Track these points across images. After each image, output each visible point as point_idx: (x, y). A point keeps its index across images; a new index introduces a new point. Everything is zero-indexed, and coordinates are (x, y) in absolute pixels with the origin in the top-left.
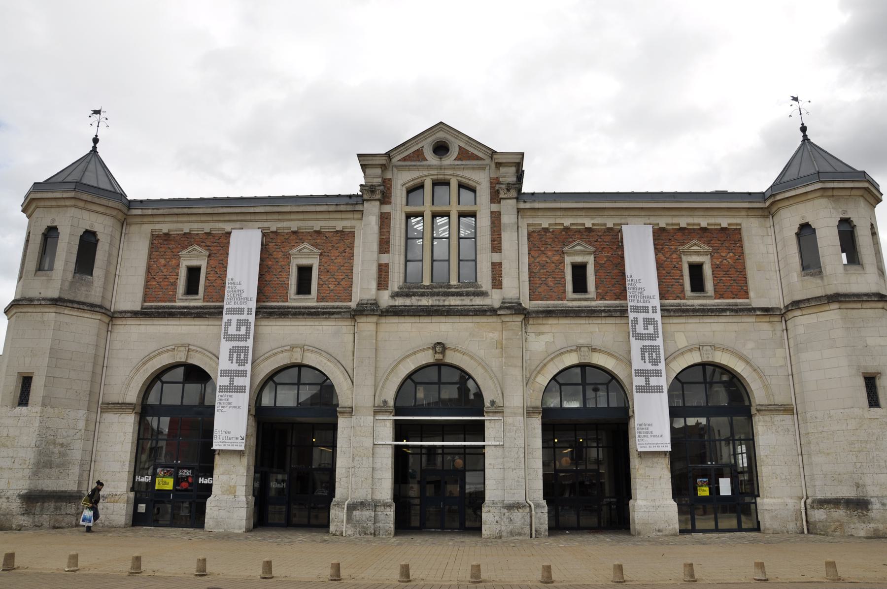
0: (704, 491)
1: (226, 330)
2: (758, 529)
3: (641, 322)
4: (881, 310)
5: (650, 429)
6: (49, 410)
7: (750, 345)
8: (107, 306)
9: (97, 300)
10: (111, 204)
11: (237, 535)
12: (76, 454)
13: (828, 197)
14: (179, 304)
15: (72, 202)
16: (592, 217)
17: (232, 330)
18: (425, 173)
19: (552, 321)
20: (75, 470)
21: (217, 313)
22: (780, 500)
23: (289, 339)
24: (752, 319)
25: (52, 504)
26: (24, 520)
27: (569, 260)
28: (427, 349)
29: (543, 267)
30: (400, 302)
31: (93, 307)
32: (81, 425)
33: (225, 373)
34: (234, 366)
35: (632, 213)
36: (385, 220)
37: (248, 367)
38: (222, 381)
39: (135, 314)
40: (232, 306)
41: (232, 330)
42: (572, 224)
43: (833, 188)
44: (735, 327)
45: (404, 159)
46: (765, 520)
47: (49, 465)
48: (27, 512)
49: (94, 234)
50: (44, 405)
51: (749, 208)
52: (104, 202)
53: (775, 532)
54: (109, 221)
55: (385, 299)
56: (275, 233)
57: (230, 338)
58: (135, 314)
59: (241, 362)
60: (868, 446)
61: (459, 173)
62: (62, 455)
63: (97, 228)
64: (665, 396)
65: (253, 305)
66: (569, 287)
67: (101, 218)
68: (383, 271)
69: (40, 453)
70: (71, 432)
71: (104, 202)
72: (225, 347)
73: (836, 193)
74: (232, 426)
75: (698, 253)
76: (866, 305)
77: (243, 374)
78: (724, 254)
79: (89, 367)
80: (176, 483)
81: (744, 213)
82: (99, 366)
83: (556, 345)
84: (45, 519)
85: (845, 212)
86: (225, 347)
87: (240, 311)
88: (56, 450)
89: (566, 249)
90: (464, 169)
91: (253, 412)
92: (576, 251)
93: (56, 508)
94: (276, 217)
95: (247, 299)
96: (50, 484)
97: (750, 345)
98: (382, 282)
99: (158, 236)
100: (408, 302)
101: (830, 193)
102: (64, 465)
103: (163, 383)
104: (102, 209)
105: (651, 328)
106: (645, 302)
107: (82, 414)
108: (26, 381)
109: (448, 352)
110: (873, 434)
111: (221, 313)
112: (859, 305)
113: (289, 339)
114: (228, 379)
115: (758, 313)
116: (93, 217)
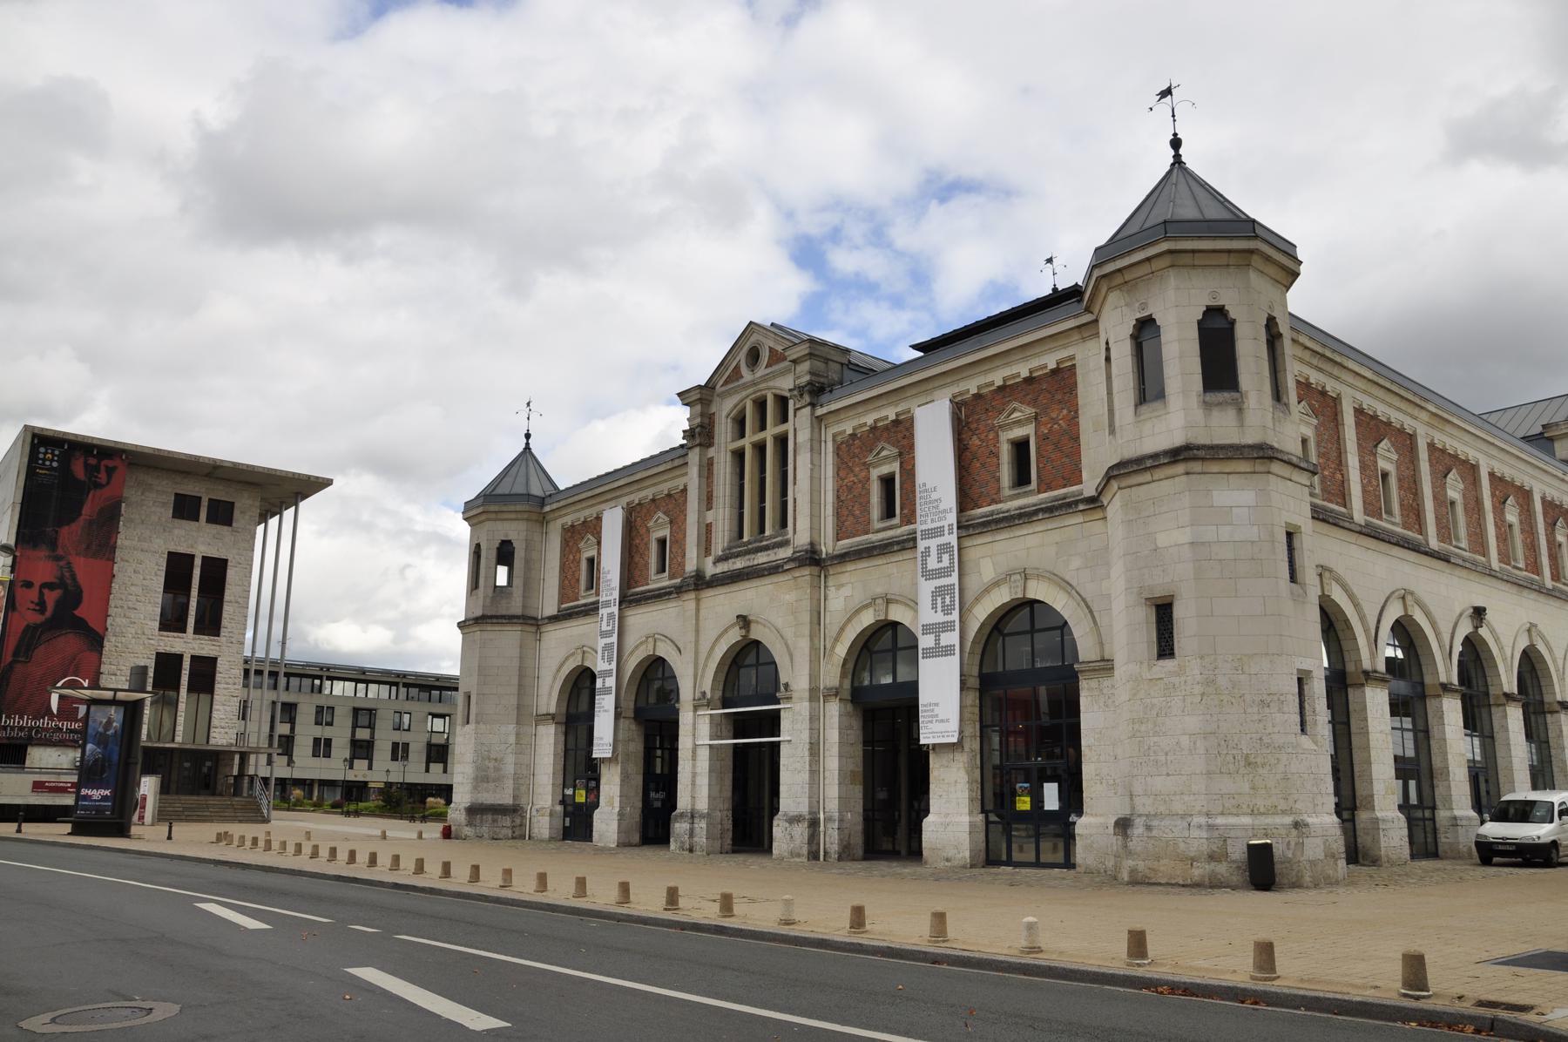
0: (1024, 804)
1: (924, 563)
2: (1069, 864)
3: (934, 552)
4: (1184, 478)
5: (937, 710)
6: (482, 726)
7: (1076, 563)
8: (532, 613)
9: (518, 612)
10: (519, 508)
11: (610, 849)
12: (509, 768)
13: (1119, 287)
14: (582, 602)
15: (483, 517)
16: (1026, 359)
17: (932, 563)
18: (744, 394)
19: (850, 567)
20: (509, 784)
21: (909, 543)
22: (1101, 820)
23: (1007, 565)
24: (1079, 519)
25: (490, 817)
26: (468, 831)
27: (875, 473)
28: (732, 626)
29: (850, 489)
30: (723, 567)
31: (510, 619)
32: (512, 739)
33: (928, 629)
34: (940, 617)
35: (937, 383)
36: (708, 468)
37: (955, 616)
38: (925, 642)
39: (554, 619)
40: (930, 526)
41: (932, 563)
42: (876, 421)
43: (1193, 251)
44: (1056, 536)
45: (726, 383)
46: (1081, 854)
47: (486, 779)
48: (470, 824)
49: (509, 543)
50: (477, 722)
51: (1078, 327)
52: (512, 508)
53: (1089, 872)
54: (522, 526)
55: (710, 569)
56: (977, 396)
57: (929, 575)
58: (554, 619)
59: (947, 610)
60: (1143, 728)
61: (771, 384)
62: (497, 769)
63: (512, 536)
64: (955, 660)
65: (952, 518)
66: (876, 510)
67: (514, 525)
68: (707, 531)
69: (478, 768)
70: (503, 747)
71: (512, 508)
72: (926, 588)
73: (1128, 276)
74: (942, 705)
75: (1018, 423)
76: (1158, 474)
77: (947, 627)
78: (1054, 415)
79: (515, 681)
80: (77, 800)
81: (1076, 336)
82: (525, 681)
83: (851, 600)
84: (485, 830)
85: (1144, 306)
86: (926, 588)
87: (938, 532)
88: (491, 765)
89: (870, 458)
90: (774, 377)
91: (974, 682)
92: (886, 457)
93: (494, 821)
94: (636, 487)
95: (945, 511)
96: (488, 798)
97: (1076, 563)
98: (706, 546)
99: (964, 403)
100: (739, 564)
101: (1118, 280)
102: (499, 779)
103: (1004, 636)
104: (513, 516)
105: (946, 557)
106: (940, 519)
107: (512, 728)
108: (1164, 612)
109: (753, 626)
110: (1153, 706)
111: (915, 539)
112: (1147, 477)
113: (1007, 565)
114: (932, 637)
115: (1081, 507)
116: (507, 525)
